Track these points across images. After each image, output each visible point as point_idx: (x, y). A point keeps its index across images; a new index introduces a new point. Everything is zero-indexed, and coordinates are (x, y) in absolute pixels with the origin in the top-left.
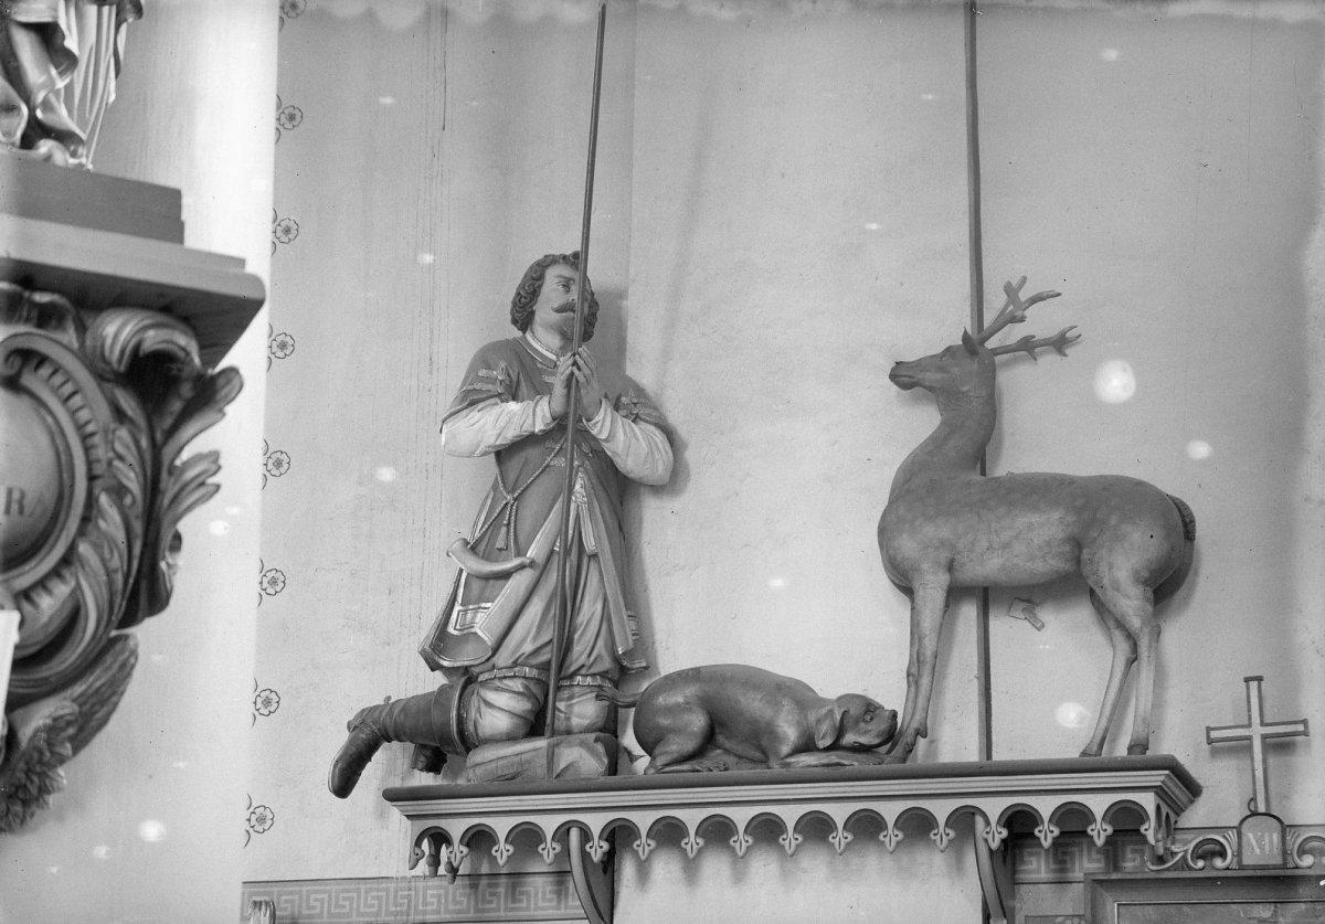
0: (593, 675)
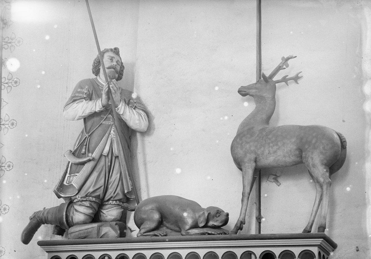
0: (116, 200)
